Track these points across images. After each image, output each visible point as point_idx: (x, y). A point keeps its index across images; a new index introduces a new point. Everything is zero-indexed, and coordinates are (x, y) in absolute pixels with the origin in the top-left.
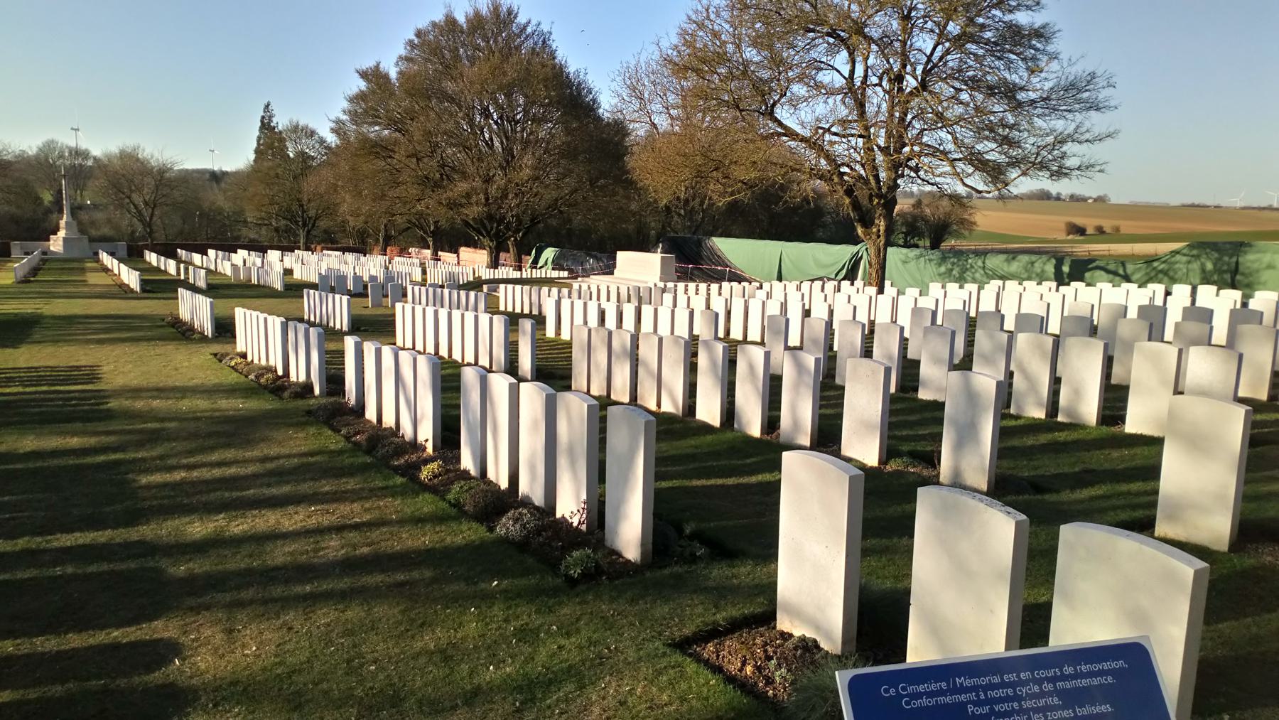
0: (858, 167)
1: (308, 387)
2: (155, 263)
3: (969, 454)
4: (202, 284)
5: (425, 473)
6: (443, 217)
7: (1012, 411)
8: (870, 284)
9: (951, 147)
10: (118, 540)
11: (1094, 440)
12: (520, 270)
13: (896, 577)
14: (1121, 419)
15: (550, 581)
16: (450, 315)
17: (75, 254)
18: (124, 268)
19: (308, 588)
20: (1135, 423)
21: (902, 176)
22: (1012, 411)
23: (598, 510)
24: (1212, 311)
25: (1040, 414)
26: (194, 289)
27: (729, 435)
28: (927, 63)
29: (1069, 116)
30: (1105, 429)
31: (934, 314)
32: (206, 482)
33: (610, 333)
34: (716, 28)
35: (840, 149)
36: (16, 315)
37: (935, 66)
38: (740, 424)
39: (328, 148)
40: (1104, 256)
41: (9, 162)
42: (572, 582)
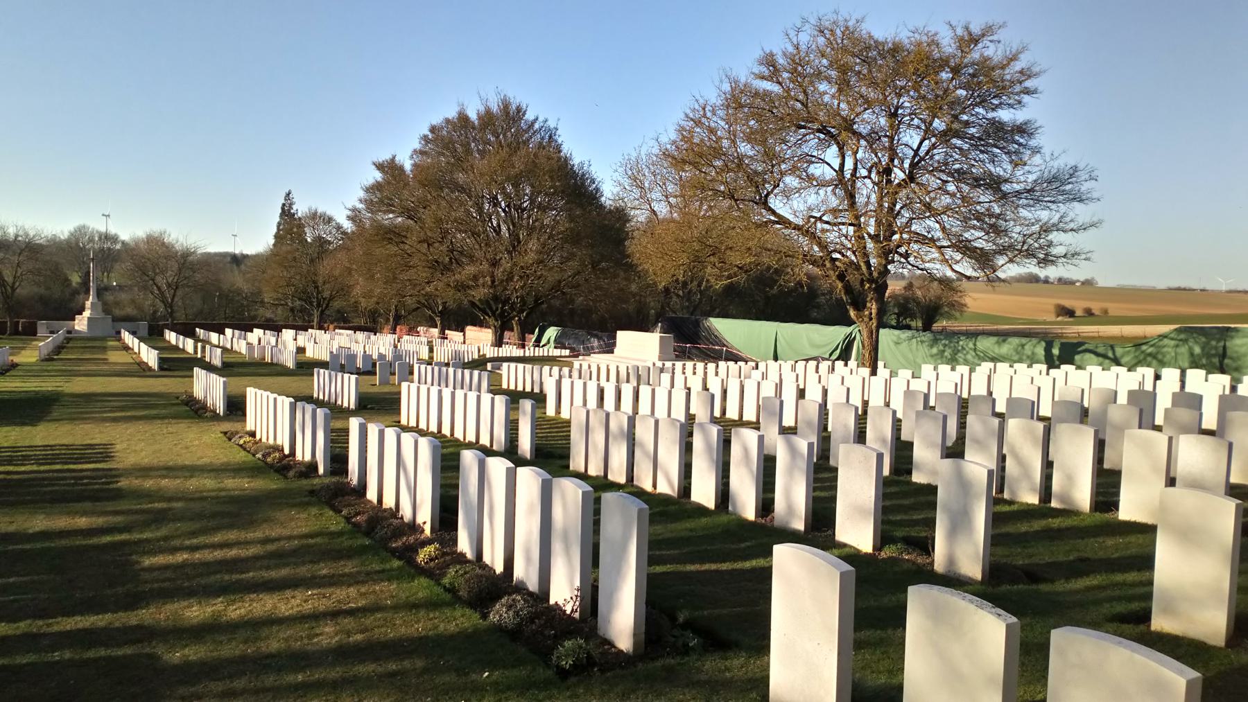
0: (849, 253)
1: (313, 466)
2: (174, 342)
3: (962, 545)
4: (217, 362)
5: (422, 556)
6: (451, 298)
7: (1006, 496)
8: (864, 365)
9: (939, 234)
10: (117, 624)
11: (1086, 527)
12: (523, 346)
13: (890, 672)
14: (1115, 506)
15: (543, 673)
16: (453, 394)
17: (99, 333)
18: (144, 347)
19: (300, 677)
20: (1129, 509)
21: (893, 262)
22: (1006, 496)
23: (591, 595)
24: (1201, 397)
25: (1033, 499)
26: (209, 368)
27: (724, 519)
28: (914, 157)
29: (1053, 206)
30: (1099, 516)
31: (927, 397)
32: (206, 564)
33: (608, 415)
34: (713, 125)
35: (832, 236)
36: (37, 393)
37: (922, 159)
38: (734, 506)
39: (345, 233)
40: (1093, 338)
41: (40, 245)
42: (563, 674)
